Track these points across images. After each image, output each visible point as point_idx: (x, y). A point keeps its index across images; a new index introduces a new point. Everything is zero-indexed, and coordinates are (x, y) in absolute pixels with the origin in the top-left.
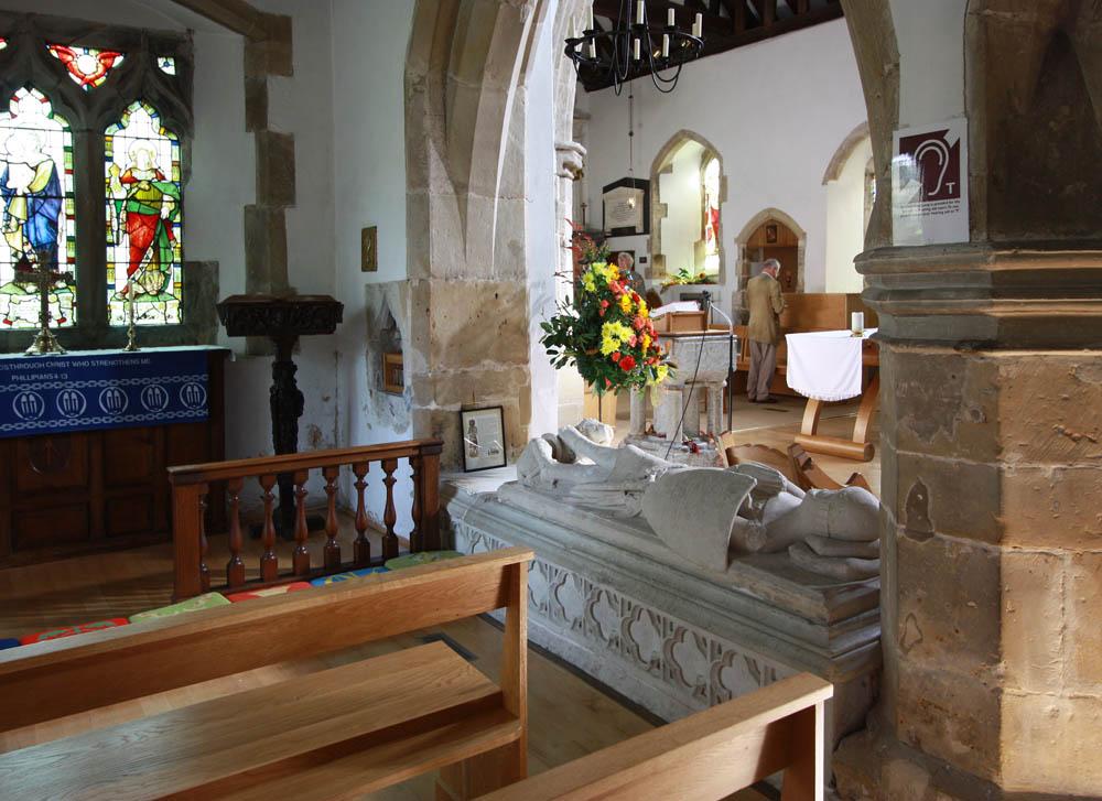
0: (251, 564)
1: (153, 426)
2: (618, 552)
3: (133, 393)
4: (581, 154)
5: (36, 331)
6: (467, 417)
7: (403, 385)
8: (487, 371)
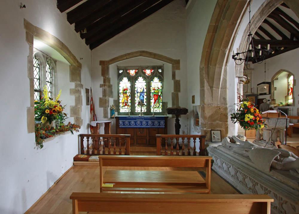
0: (169, 152)
1: (156, 128)
2: (242, 163)
3: (153, 123)
4: (245, 78)
5: (140, 113)
6: (212, 132)
7: (199, 124)
8: (217, 123)
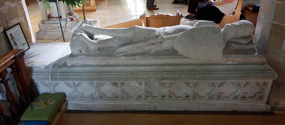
6: (8, 33)
